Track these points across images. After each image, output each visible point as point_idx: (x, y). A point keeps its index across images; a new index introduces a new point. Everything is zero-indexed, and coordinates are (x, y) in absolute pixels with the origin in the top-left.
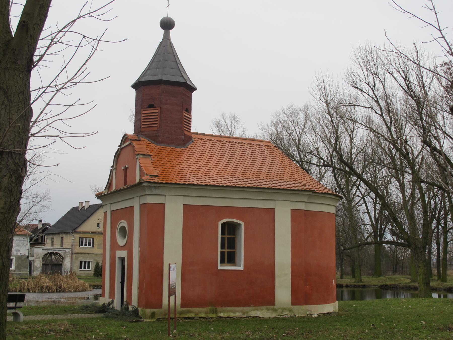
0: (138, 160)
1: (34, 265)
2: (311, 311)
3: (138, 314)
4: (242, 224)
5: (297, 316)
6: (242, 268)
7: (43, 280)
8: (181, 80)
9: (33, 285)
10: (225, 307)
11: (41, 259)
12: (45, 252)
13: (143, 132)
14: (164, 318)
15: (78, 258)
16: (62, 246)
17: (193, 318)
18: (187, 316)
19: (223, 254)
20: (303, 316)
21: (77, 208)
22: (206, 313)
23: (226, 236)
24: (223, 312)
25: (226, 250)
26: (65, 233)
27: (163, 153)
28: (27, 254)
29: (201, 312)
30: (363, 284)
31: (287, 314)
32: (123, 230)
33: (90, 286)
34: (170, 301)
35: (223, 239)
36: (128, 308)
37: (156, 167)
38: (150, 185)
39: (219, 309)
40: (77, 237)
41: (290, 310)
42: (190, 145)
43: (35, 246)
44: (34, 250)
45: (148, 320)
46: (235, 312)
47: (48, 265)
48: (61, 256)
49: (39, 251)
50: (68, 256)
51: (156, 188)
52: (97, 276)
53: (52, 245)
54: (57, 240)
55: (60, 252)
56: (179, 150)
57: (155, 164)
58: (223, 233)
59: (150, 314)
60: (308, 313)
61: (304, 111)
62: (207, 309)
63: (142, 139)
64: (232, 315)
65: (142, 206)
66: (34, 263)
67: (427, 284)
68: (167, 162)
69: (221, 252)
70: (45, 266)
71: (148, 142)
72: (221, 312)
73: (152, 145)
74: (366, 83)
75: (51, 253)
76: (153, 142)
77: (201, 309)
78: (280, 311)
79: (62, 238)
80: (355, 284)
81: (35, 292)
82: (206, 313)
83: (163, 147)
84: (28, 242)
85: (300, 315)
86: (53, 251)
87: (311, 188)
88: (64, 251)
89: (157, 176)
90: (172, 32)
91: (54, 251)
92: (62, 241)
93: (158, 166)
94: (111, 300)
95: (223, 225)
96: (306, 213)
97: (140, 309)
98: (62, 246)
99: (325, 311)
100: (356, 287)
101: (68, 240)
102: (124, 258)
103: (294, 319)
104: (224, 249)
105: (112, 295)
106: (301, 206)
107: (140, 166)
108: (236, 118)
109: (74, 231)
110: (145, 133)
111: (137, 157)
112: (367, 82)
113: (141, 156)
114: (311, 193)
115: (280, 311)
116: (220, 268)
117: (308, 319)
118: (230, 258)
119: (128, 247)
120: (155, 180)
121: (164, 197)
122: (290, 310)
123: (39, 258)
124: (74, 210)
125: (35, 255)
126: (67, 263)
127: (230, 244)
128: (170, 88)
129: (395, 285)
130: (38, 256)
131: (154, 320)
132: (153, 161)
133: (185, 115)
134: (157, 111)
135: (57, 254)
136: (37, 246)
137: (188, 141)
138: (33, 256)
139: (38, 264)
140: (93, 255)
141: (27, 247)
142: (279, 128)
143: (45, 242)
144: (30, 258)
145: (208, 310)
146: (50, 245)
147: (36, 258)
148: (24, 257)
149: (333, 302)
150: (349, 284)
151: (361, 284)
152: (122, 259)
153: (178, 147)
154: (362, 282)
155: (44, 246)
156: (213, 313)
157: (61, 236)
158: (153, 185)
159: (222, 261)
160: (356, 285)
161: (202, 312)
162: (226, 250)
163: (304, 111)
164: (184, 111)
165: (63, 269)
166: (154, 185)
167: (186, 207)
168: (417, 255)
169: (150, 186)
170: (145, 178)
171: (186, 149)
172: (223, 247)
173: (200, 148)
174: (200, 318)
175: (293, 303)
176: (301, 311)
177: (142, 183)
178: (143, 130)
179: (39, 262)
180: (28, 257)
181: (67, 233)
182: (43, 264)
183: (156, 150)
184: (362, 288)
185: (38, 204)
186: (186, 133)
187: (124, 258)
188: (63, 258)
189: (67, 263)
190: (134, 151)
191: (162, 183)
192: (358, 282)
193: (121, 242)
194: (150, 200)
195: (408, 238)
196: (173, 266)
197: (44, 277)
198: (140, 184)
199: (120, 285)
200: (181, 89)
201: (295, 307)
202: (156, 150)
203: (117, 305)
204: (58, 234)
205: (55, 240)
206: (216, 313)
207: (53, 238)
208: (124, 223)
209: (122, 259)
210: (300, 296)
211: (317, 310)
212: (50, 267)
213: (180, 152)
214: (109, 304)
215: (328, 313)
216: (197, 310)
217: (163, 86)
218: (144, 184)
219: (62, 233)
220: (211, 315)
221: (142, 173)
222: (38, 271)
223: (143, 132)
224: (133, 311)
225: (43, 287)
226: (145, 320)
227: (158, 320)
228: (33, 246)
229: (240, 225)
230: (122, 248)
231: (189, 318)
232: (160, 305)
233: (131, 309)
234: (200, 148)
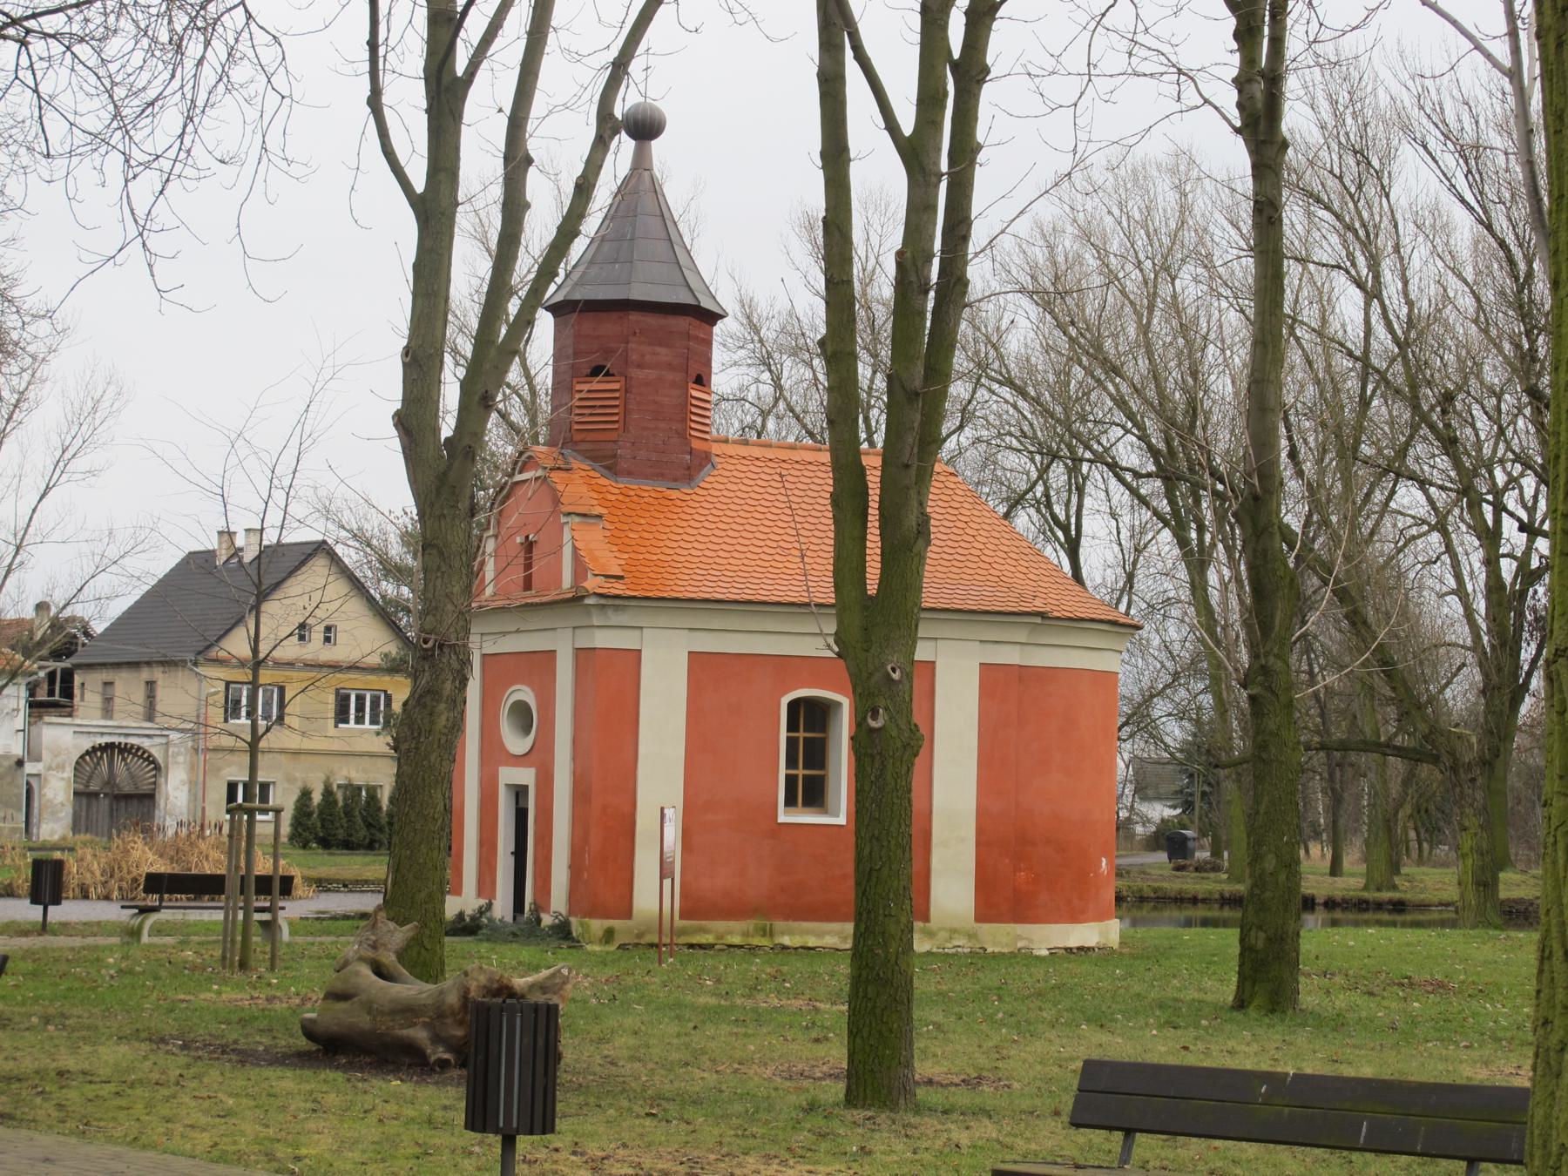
0: (566, 529)
1: (41, 796)
2: (1031, 941)
3: (569, 933)
4: (846, 703)
5: (990, 950)
6: (841, 820)
7: (136, 854)
8: (684, 298)
9: (98, 873)
10: (795, 920)
11: (69, 773)
12: (87, 743)
13: (576, 443)
14: (637, 945)
15: (219, 769)
16: (150, 715)
17: (712, 946)
18: (694, 942)
19: (791, 781)
20: (1005, 950)
21: (210, 555)
22: (746, 934)
23: (801, 735)
24: (791, 933)
25: (801, 772)
26: (162, 663)
27: (634, 506)
28: (17, 750)
29: (731, 933)
30: (1396, 895)
31: (962, 944)
32: (522, 714)
33: (309, 881)
34: (650, 894)
35: (792, 743)
36: (539, 920)
37: (615, 548)
38: (603, 601)
39: (779, 925)
40: (213, 680)
41: (971, 936)
42: (708, 478)
43: (47, 719)
44: (40, 735)
45: (597, 948)
46: (820, 935)
47: (96, 795)
48: (150, 760)
49: (64, 739)
50: (181, 759)
51: (617, 608)
52: (305, 846)
53: (108, 712)
54: (129, 687)
55: (145, 743)
56: (674, 494)
57: (617, 540)
58: (792, 726)
59: (600, 933)
60: (1020, 945)
61: (1174, 171)
62: (749, 924)
63: (575, 464)
64: (812, 942)
65: (583, 656)
66: (40, 789)
67: (1485, 885)
68: (646, 535)
69: (787, 776)
70: (84, 801)
71: (592, 474)
72: (783, 933)
73: (603, 481)
74: (1331, 172)
75: (110, 747)
76: (605, 472)
77: (732, 924)
78: (943, 935)
79: (150, 684)
80: (1366, 895)
81: (107, 898)
82: (746, 934)
83: (633, 485)
84: (23, 703)
85: (997, 950)
86: (116, 740)
87: (1038, 605)
88: (163, 740)
89: (621, 577)
90: (656, 145)
91: (123, 740)
92: (151, 697)
93: (622, 547)
94: (483, 902)
95: (794, 706)
96: (1023, 673)
97: (574, 921)
98: (150, 715)
99: (1073, 943)
100: (1366, 910)
101: (183, 695)
102: (526, 787)
103: (980, 959)
104: (795, 767)
105: (486, 885)
106: (1010, 656)
107: (575, 548)
108: (887, 206)
109: (205, 653)
110: (583, 446)
111: (563, 519)
112: (1337, 171)
113: (577, 519)
114: (1038, 620)
115: (943, 935)
116: (783, 818)
117: (1022, 957)
118: (812, 793)
119: (540, 757)
120: (618, 588)
121: (637, 632)
122: (971, 936)
123: (61, 767)
124: (197, 565)
125: (45, 755)
126: (176, 789)
127: (810, 753)
128: (651, 321)
129: (1519, 901)
130: (59, 760)
131: (612, 948)
132: (608, 533)
133: (694, 393)
134: (617, 386)
135: (125, 750)
136: (54, 719)
137: (702, 467)
138: (38, 759)
139: (58, 790)
140: (282, 758)
141: (19, 722)
142: (1068, 243)
143: (77, 699)
144: (29, 768)
145: (751, 928)
146: (99, 713)
147: (50, 768)
148: (6, 764)
149: (1101, 917)
150: (1338, 895)
151: (1386, 895)
152: (519, 792)
153: (673, 485)
154: (1395, 887)
155: (70, 715)
156: (764, 935)
157: (145, 674)
158: (610, 602)
159: (790, 801)
160: (1366, 902)
161: (734, 931)
162: (801, 772)
163: (1174, 171)
164: (691, 385)
165: (159, 813)
166: (613, 602)
167: (697, 660)
168: (1458, 790)
169: (603, 606)
170: (591, 584)
171: (697, 490)
172: (791, 762)
173: (735, 487)
174: (730, 946)
175: (981, 917)
176: (1001, 937)
177: (583, 597)
178: (577, 437)
179: (62, 784)
180: (20, 763)
181: (169, 664)
182: (76, 793)
183: (613, 498)
184: (1390, 912)
185: (114, 568)
186: (695, 444)
187: (526, 787)
188: (157, 768)
189: (176, 789)
190: (557, 501)
191: (634, 597)
192: (1379, 890)
193: (517, 744)
194: (604, 640)
195: (1431, 732)
196: (669, 813)
197: (140, 844)
198: (576, 600)
199: (512, 860)
200: (683, 323)
201: (986, 926)
202: (613, 498)
203: (502, 908)
204: (134, 665)
205: (119, 690)
206: (771, 936)
207: (108, 684)
208: (525, 694)
209: (519, 792)
210: (999, 897)
211: (1048, 937)
212: (104, 804)
213: (679, 503)
214: (481, 912)
215: (1080, 949)
216: (720, 925)
217: (634, 316)
218: (589, 601)
219: (149, 664)
220: (756, 941)
221: (580, 570)
222: (58, 820)
223: (576, 443)
224: (552, 927)
225: (135, 880)
226: (589, 947)
227: (621, 947)
228: (40, 717)
229: (839, 704)
230: (518, 760)
231: (701, 946)
232: (627, 913)
233: (547, 920)
234: (735, 487)
